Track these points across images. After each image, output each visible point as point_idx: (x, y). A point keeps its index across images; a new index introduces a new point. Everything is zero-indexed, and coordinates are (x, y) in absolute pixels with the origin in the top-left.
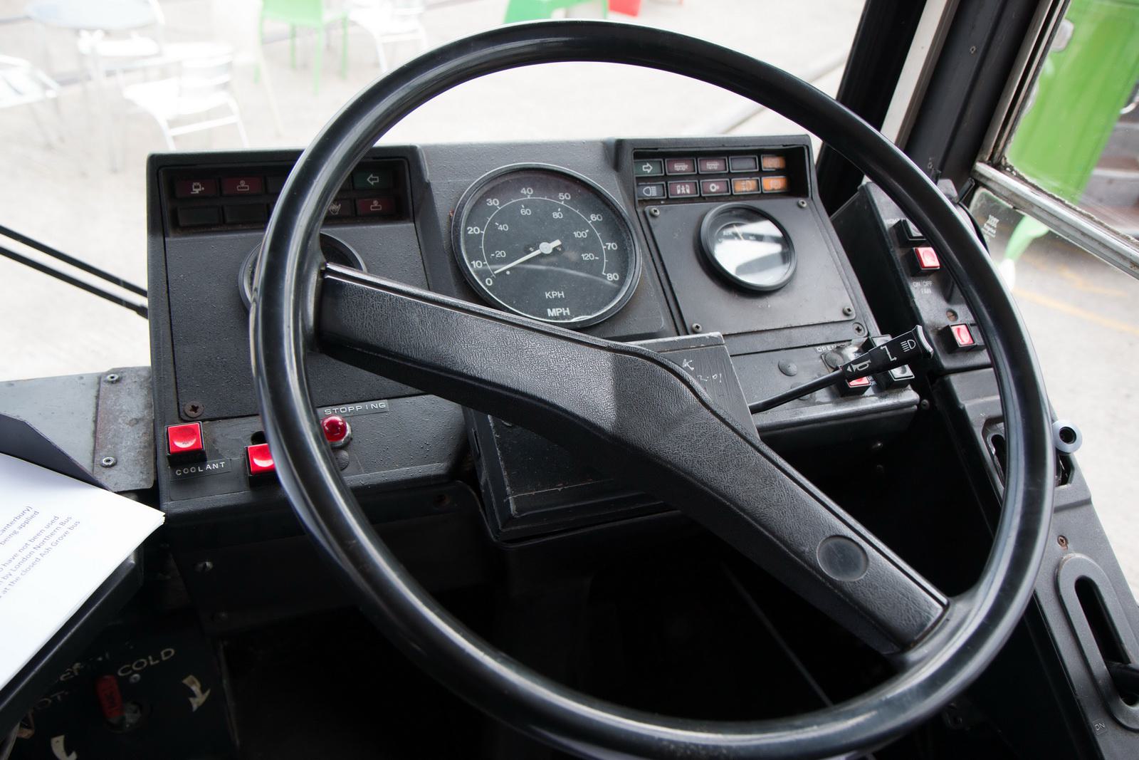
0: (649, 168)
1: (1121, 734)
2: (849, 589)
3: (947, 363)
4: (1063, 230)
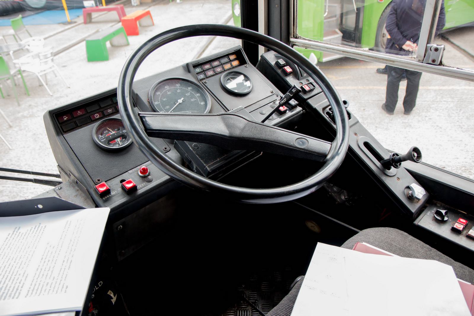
0: (198, 70)
1: (389, 178)
2: (306, 148)
3: (305, 97)
4: (321, 50)
